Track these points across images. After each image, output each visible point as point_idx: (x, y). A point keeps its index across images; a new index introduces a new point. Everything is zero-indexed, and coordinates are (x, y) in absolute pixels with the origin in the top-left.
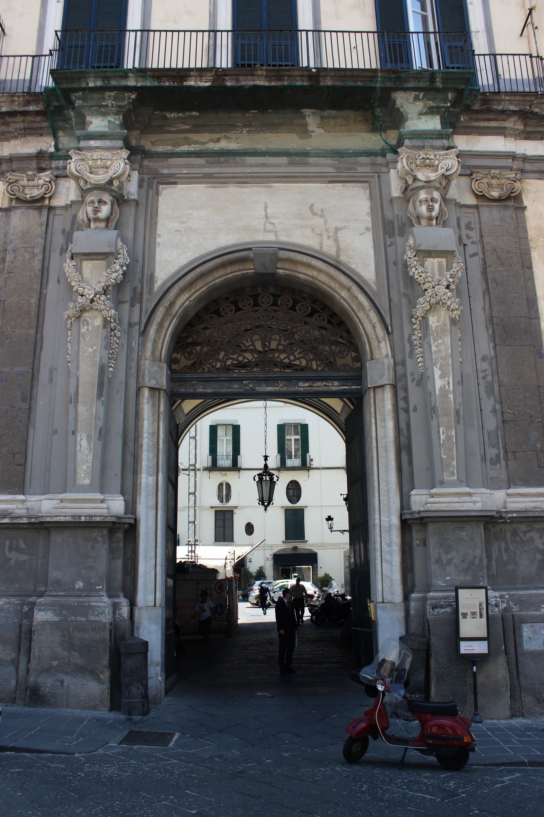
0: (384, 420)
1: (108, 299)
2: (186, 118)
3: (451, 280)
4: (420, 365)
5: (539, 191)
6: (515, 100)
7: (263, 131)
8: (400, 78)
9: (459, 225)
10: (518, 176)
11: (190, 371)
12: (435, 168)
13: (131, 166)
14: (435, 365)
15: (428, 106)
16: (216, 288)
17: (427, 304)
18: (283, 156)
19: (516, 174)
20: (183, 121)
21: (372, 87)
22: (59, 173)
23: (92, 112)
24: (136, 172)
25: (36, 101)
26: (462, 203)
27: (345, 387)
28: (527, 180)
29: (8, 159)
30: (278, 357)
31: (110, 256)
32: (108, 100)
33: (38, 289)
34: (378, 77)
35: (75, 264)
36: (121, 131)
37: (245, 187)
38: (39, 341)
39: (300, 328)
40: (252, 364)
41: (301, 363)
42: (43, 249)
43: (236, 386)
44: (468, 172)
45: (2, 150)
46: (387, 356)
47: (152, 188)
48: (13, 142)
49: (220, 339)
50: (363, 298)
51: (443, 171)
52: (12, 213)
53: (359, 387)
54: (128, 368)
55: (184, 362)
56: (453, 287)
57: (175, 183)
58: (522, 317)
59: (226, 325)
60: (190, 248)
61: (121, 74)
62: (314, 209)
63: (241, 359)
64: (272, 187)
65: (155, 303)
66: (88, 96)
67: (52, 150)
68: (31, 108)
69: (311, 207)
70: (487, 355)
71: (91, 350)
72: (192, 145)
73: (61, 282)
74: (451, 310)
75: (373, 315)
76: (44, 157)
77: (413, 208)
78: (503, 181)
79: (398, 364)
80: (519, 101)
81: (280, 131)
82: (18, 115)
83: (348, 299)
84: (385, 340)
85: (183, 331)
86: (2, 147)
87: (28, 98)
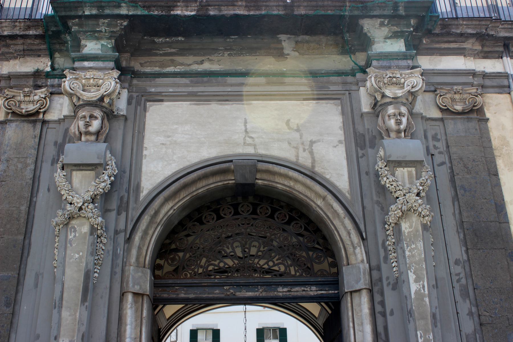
0: (362, 324)
1: (96, 207)
2: (172, 42)
3: (421, 188)
4: (395, 269)
5: (500, 104)
6: (472, 25)
7: (242, 54)
8: (366, 7)
9: (426, 137)
10: (479, 91)
11: (173, 277)
12: (401, 86)
13: (121, 85)
14: (410, 269)
15: (392, 31)
16: (199, 198)
17: (399, 211)
18: (261, 77)
19: (477, 89)
20: (169, 45)
21: (342, 15)
22: (54, 90)
23: (87, 37)
24: (126, 90)
25: (36, 26)
26: (428, 116)
27: (323, 292)
28: (488, 95)
29: (7, 77)
30: (258, 263)
31: (99, 167)
32: (102, 26)
33: (28, 197)
34: (346, 6)
35: (65, 174)
36: (113, 54)
37: (226, 105)
38: (27, 246)
39: (279, 235)
40: (232, 270)
41: (280, 269)
42: (35, 159)
43: (217, 291)
44: (432, 89)
45: (1, 69)
46: (362, 261)
47: (140, 105)
48: (12, 62)
49: (202, 246)
50: (338, 206)
51: (409, 88)
52: (7, 126)
53: (336, 292)
54: (113, 273)
55: (168, 268)
56: (423, 194)
57: (162, 101)
58: (491, 222)
59: (208, 233)
60: (174, 160)
61: (115, 4)
62: (290, 124)
63: (222, 265)
64: (251, 104)
65: (140, 211)
66: (84, 23)
67: (48, 69)
68: (31, 33)
69: (288, 122)
70: (459, 259)
71: (77, 256)
72: (178, 67)
73: (51, 191)
74: (422, 216)
75: (348, 222)
76: (41, 75)
77: (383, 122)
78: (465, 96)
79: (374, 269)
80: (475, 25)
81: (258, 54)
82: (19, 38)
83: (323, 207)
84: (360, 246)
85: (168, 237)
86: (2, 66)
87: (28, 23)
